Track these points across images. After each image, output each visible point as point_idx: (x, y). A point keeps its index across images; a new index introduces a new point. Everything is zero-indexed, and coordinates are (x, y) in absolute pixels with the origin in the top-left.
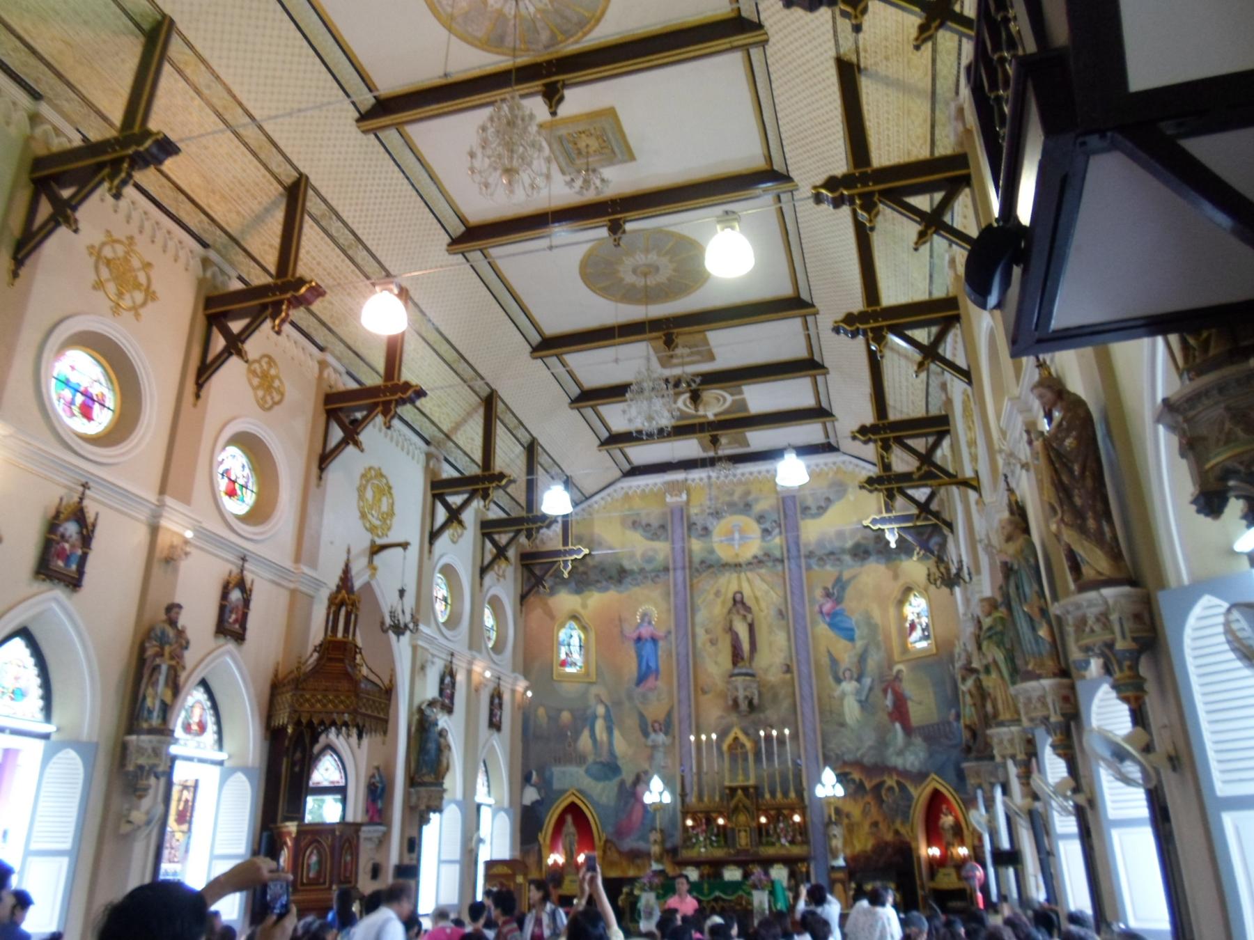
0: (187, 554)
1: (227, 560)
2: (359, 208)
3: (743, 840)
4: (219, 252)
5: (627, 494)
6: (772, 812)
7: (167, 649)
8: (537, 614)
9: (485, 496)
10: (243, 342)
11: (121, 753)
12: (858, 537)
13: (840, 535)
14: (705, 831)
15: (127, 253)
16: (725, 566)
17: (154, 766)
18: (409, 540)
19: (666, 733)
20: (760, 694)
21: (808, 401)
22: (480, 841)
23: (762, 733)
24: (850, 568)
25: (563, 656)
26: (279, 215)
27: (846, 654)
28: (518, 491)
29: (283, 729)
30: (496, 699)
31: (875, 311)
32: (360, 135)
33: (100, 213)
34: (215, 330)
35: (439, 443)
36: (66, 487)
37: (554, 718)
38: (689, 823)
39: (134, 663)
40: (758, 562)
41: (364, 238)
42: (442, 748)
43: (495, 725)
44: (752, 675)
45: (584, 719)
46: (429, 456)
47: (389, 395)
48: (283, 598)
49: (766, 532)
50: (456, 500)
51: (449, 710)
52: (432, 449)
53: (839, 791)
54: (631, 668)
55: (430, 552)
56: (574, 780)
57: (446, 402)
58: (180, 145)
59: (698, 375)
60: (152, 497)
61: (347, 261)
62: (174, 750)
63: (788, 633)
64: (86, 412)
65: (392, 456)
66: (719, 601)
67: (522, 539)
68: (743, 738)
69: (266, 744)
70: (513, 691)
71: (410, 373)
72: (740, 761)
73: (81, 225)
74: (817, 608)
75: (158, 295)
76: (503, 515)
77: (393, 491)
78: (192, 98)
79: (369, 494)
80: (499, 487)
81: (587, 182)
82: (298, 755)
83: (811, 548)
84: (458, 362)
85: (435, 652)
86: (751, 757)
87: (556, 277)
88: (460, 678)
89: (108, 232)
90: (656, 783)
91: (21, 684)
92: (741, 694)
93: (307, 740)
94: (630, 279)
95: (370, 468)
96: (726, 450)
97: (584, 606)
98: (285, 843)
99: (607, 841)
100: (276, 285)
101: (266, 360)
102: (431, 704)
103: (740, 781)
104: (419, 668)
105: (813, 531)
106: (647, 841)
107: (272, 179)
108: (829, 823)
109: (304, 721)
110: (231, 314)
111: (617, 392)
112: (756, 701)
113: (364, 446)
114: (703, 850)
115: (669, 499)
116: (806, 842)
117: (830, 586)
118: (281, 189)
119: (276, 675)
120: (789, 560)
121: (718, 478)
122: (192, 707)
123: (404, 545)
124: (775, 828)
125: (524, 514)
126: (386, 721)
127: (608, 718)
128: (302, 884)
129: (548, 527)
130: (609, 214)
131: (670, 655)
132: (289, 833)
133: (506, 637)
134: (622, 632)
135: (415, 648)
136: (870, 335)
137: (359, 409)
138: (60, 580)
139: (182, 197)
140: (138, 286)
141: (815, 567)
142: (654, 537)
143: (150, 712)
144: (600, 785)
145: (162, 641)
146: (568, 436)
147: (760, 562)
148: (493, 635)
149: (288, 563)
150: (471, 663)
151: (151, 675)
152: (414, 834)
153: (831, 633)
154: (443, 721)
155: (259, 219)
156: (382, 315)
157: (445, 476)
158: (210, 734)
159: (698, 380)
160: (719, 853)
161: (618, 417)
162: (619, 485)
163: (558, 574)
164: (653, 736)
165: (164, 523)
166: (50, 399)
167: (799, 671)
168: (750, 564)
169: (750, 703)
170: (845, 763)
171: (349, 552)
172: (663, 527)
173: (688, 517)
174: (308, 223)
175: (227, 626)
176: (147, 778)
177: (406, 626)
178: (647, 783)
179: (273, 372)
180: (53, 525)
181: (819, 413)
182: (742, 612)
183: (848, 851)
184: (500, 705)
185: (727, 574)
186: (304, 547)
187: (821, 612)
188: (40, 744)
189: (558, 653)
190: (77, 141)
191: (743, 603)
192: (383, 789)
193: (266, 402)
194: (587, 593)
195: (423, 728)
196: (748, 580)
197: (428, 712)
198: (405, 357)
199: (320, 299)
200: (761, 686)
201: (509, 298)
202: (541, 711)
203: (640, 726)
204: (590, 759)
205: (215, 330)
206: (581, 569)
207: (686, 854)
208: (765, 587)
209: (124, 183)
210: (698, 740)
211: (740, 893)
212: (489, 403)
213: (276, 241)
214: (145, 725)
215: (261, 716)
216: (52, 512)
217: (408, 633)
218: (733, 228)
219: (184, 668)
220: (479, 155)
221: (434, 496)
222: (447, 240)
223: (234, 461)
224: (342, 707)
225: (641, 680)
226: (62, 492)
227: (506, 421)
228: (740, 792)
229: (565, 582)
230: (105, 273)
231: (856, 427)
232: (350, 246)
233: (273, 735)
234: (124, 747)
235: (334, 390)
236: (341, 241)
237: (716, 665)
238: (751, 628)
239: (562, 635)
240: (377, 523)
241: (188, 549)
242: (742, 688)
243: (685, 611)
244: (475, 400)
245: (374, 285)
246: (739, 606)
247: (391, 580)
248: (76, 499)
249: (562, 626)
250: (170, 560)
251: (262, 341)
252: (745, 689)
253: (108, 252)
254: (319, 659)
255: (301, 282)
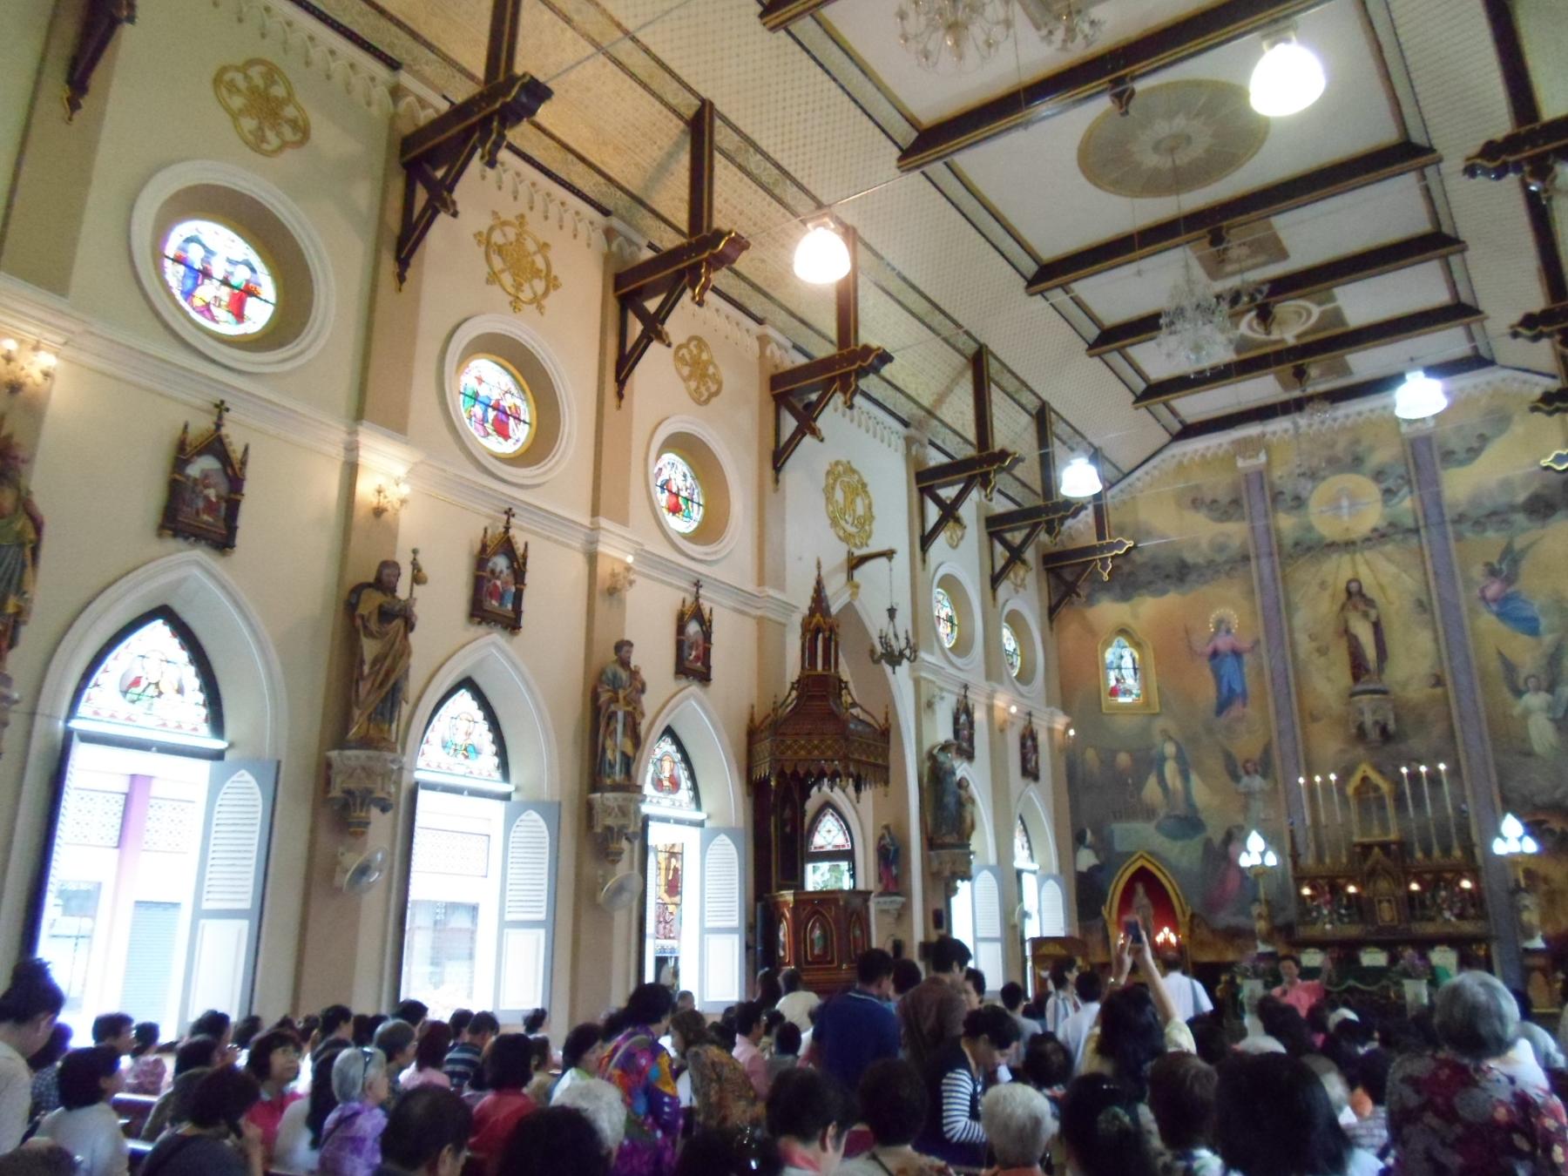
0: (631, 583)
1: (679, 588)
2: (780, 130)
3: (1386, 913)
4: (622, 218)
5: (1180, 463)
6: (1428, 877)
7: (621, 694)
8: (1071, 628)
9: (985, 483)
10: (663, 322)
11: (588, 813)
12: (1535, 486)
13: (1506, 485)
14: (1330, 902)
15: (519, 235)
16: (1332, 546)
17: (622, 828)
18: (894, 547)
19: (1265, 776)
20: (1397, 719)
21: (1439, 296)
22: (1025, 915)
23: (1404, 770)
24: (1526, 532)
25: (1113, 683)
26: (685, 159)
27: (1527, 653)
28: (1028, 470)
29: (766, 781)
30: (1028, 740)
31: (1533, 131)
32: (767, 35)
33: (484, 191)
34: (631, 317)
35: (920, 422)
36: (489, 517)
37: (1108, 760)
38: (1306, 891)
39: (588, 715)
40: (1379, 537)
41: (791, 170)
42: (963, 802)
43: (1030, 772)
44: (1384, 692)
45: (1149, 762)
46: (909, 441)
47: (848, 366)
48: (750, 626)
49: (1388, 493)
50: (948, 493)
51: (969, 756)
52: (912, 431)
53: (1530, 846)
54: (1207, 692)
55: (924, 561)
56: (1141, 839)
57: (919, 367)
58: (550, 85)
59: (1263, 283)
60: (585, 520)
61: (775, 204)
62: (646, 809)
63: (1435, 631)
64: (503, 432)
65: (863, 446)
66: (1326, 595)
67: (1043, 537)
68: (1375, 777)
69: (750, 801)
70: (1051, 730)
71: (870, 335)
72: (1374, 808)
73: (460, 207)
74: (1477, 592)
75: (561, 280)
76: (1013, 507)
77: (869, 488)
78: (563, 31)
79: (839, 495)
80: (1002, 469)
81: (1071, 32)
82: (787, 813)
83: (1460, 509)
84: (932, 314)
85: (942, 684)
86: (1390, 803)
87: (1046, 176)
88: (979, 715)
89: (495, 213)
90: (1255, 842)
91: (474, 740)
92: (1368, 719)
93: (797, 797)
94: (1152, 160)
95: (837, 463)
96: (1319, 383)
97: (1135, 616)
98: (783, 915)
99: (1193, 916)
100: (690, 244)
101: (694, 343)
102: (945, 748)
103: (1376, 835)
104: (926, 706)
105: (1459, 485)
106: (1249, 915)
107: (670, 115)
108: (1517, 889)
109: (788, 772)
110: (644, 292)
111: (1146, 326)
112: (1392, 727)
113: (824, 433)
114: (1328, 927)
115: (1240, 463)
116: (1482, 915)
117: (1494, 560)
118: (682, 125)
119: (752, 720)
120: (1427, 529)
121: (1310, 426)
122: (661, 760)
123: (889, 554)
124: (1433, 897)
125: (1040, 502)
126: (887, 769)
127: (1180, 758)
128: (807, 962)
129: (1075, 514)
130: (1107, 74)
131: (1260, 673)
132: (786, 903)
133: (1034, 665)
134: (1190, 648)
135: (917, 682)
136: (1527, 168)
137: (812, 389)
138: (496, 622)
139: (570, 157)
140: (536, 273)
141: (1469, 535)
142: (1225, 516)
143: (612, 766)
144: (1179, 844)
145: (615, 684)
146: (1086, 391)
147: (1383, 536)
148: (1018, 662)
149: (751, 587)
150: (991, 696)
151: (608, 724)
152: (941, 905)
153: (1503, 629)
154: (962, 769)
155: (663, 168)
156: (818, 260)
157: (932, 463)
158: (685, 793)
159: (1266, 289)
160: (1353, 931)
161: (1158, 358)
162: (1167, 453)
163: (1095, 579)
164: (1245, 780)
165: (602, 548)
166: (460, 419)
167: (1455, 683)
168: (1368, 539)
169: (1384, 730)
170: (1537, 808)
171: (819, 566)
172: (1236, 502)
173: (1272, 485)
174: (720, 162)
175: (687, 664)
176: (619, 840)
177: (901, 655)
178: (1244, 840)
179: (705, 356)
180: (481, 560)
181: (1459, 311)
182: (1362, 607)
183: (1550, 929)
184: (1035, 748)
185: (1335, 556)
186: (767, 566)
187: (1484, 598)
188: (500, 806)
189: (1107, 679)
190: (444, 107)
191: (1360, 593)
192: (897, 851)
193: (701, 395)
194: (1136, 600)
195: (937, 780)
196: (1367, 563)
197: (941, 758)
198: (862, 316)
199: (744, 253)
200: (1400, 710)
201: (986, 217)
202: (1090, 754)
203: (1227, 766)
204: (1162, 813)
205: (631, 317)
206: (1126, 568)
207: (1303, 932)
208: (1392, 569)
209: (497, 146)
210: (1310, 784)
211: (1384, 982)
212: (979, 363)
213: (685, 193)
214: (608, 781)
215: (740, 772)
216: (478, 546)
217: (905, 662)
218: (1287, 40)
219: (643, 715)
220: (912, 14)
221: (922, 491)
222: (896, 153)
223: (674, 469)
224: (830, 753)
225: (1223, 706)
226: (486, 522)
227: (1004, 383)
228: (1376, 850)
229: (1106, 587)
230: (498, 263)
231: (1516, 317)
232: (776, 183)
233: (756, 789)
234: (589, 808)
235: (781, 370)
236: (764, 179)
237: (1328, 681)
238: (1377, 627)
239: (1110, 655)
240: (853, 530)
241: (632, 577)
242: (1369, 711)
243: (1276, 613)
244: (959, 360)
245: (804, 222)
246: (1356, 599)
247: (880, 596)
248: (502, 530)
249: (1108, 644)
250: (613, 591)
251: (684, 320)
252: (1374, 712)
253: (497, 238)
254: (798, 697)
255: (719, 235)
